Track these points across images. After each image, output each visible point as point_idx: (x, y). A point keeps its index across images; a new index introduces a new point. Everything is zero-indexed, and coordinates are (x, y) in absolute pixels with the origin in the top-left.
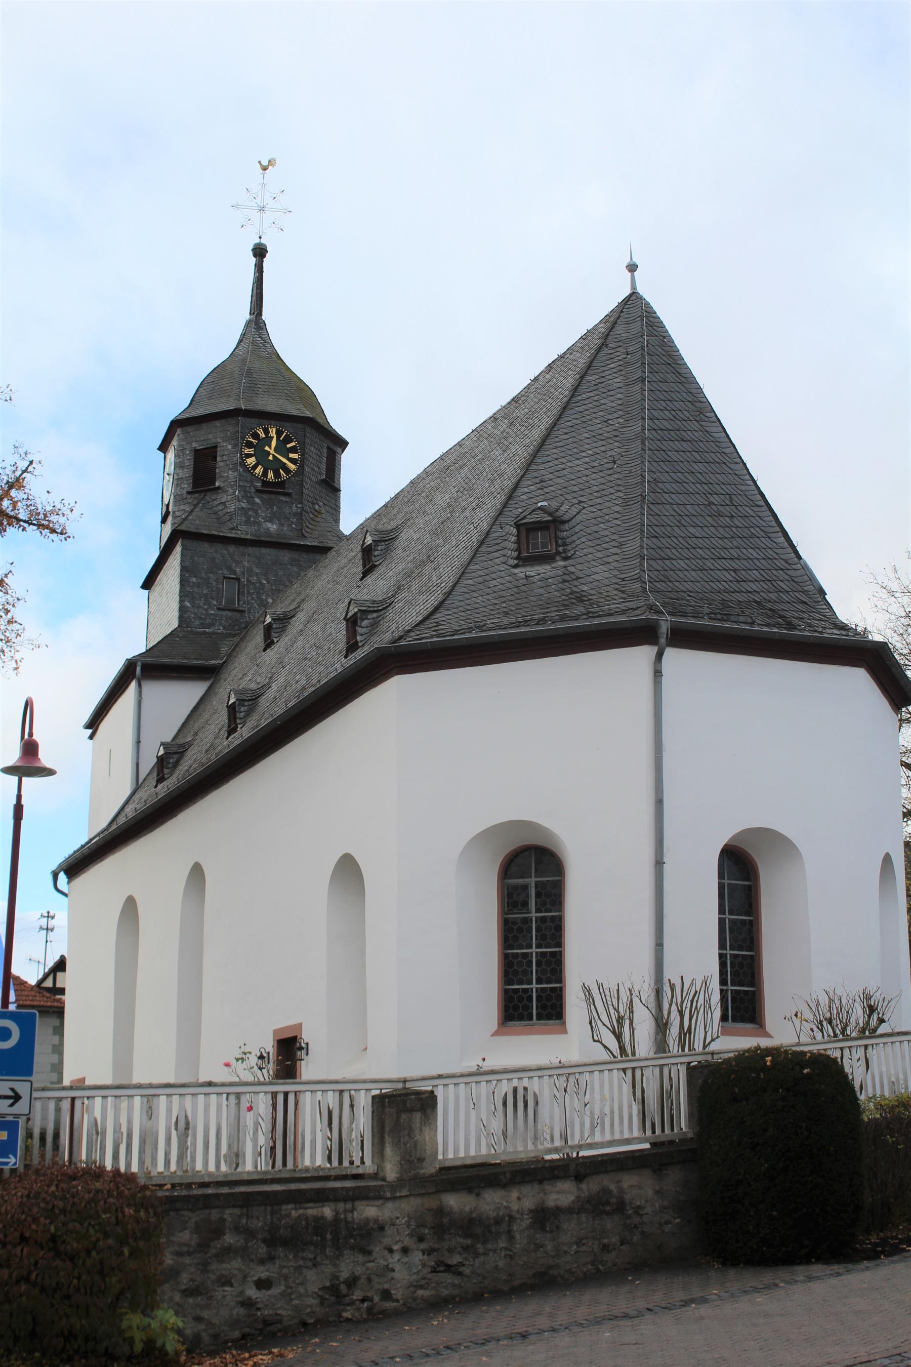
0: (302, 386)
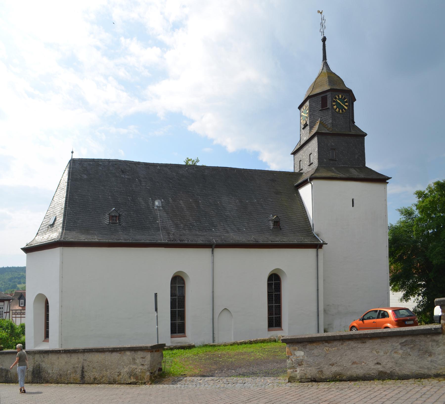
0: (114, 163)
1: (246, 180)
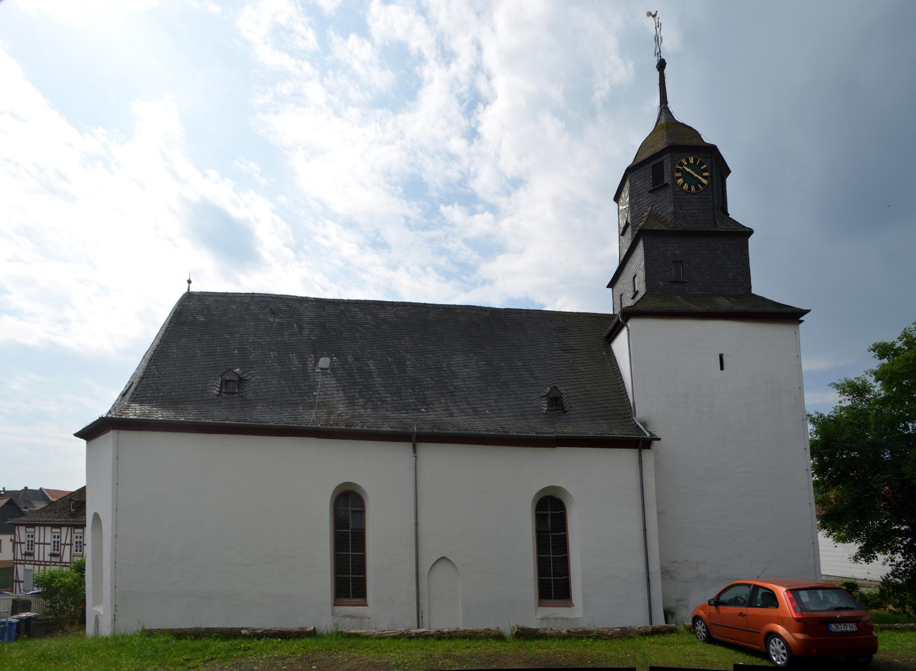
1: (506, 330)
